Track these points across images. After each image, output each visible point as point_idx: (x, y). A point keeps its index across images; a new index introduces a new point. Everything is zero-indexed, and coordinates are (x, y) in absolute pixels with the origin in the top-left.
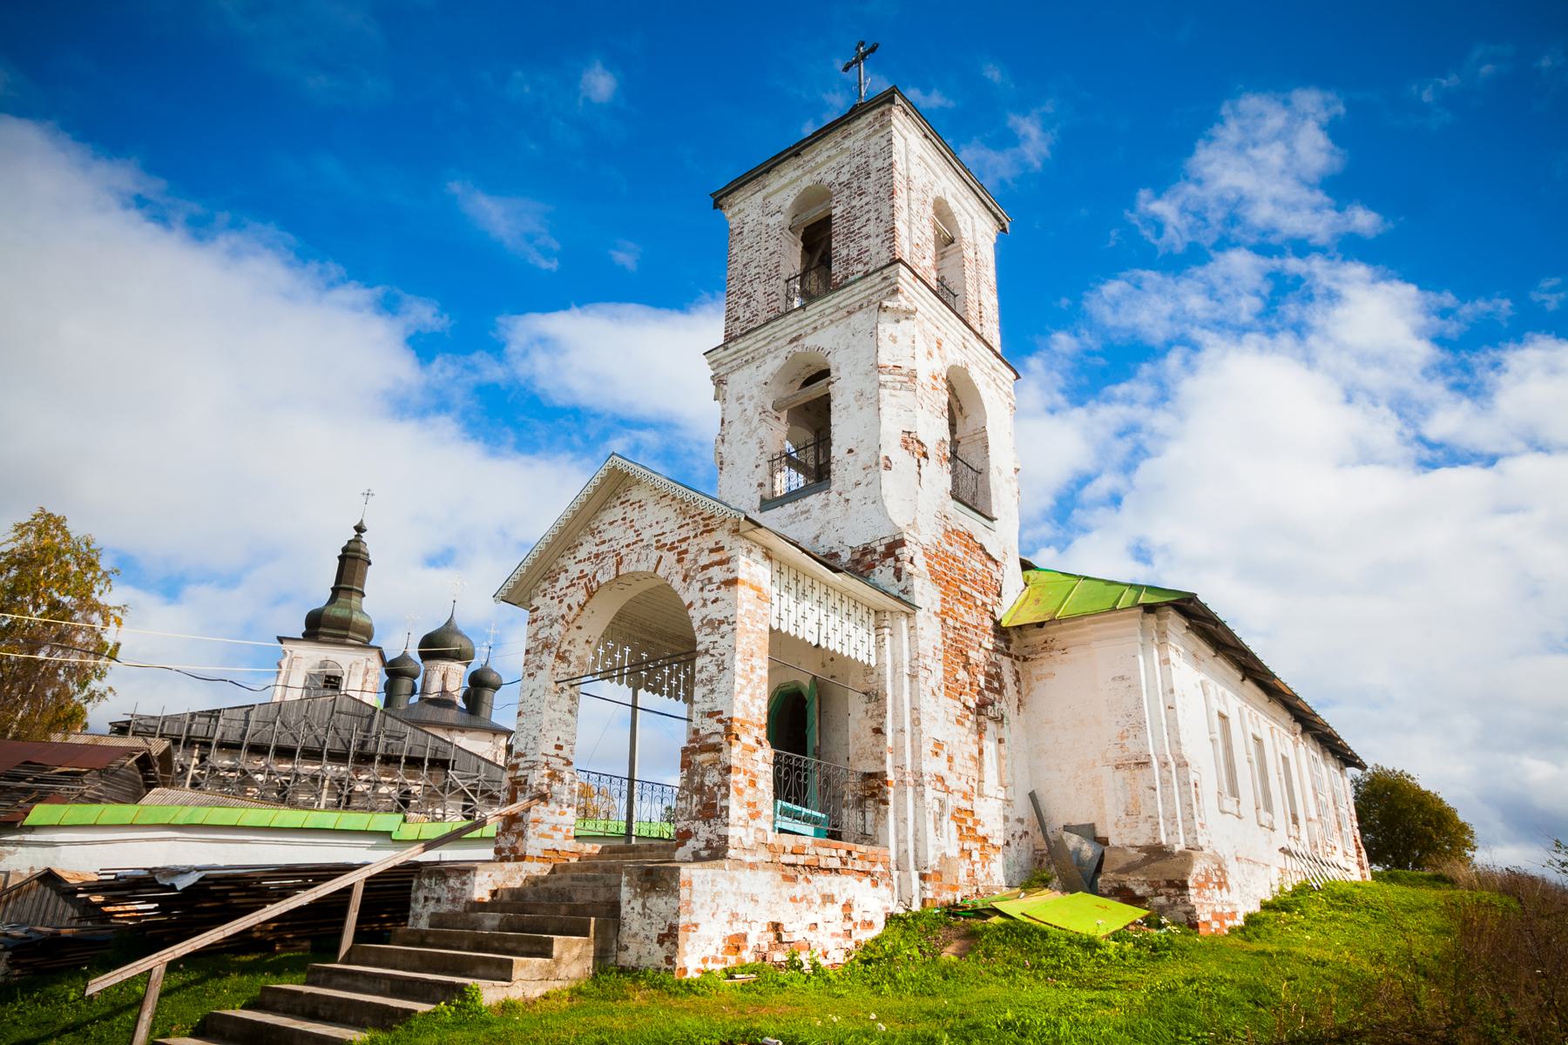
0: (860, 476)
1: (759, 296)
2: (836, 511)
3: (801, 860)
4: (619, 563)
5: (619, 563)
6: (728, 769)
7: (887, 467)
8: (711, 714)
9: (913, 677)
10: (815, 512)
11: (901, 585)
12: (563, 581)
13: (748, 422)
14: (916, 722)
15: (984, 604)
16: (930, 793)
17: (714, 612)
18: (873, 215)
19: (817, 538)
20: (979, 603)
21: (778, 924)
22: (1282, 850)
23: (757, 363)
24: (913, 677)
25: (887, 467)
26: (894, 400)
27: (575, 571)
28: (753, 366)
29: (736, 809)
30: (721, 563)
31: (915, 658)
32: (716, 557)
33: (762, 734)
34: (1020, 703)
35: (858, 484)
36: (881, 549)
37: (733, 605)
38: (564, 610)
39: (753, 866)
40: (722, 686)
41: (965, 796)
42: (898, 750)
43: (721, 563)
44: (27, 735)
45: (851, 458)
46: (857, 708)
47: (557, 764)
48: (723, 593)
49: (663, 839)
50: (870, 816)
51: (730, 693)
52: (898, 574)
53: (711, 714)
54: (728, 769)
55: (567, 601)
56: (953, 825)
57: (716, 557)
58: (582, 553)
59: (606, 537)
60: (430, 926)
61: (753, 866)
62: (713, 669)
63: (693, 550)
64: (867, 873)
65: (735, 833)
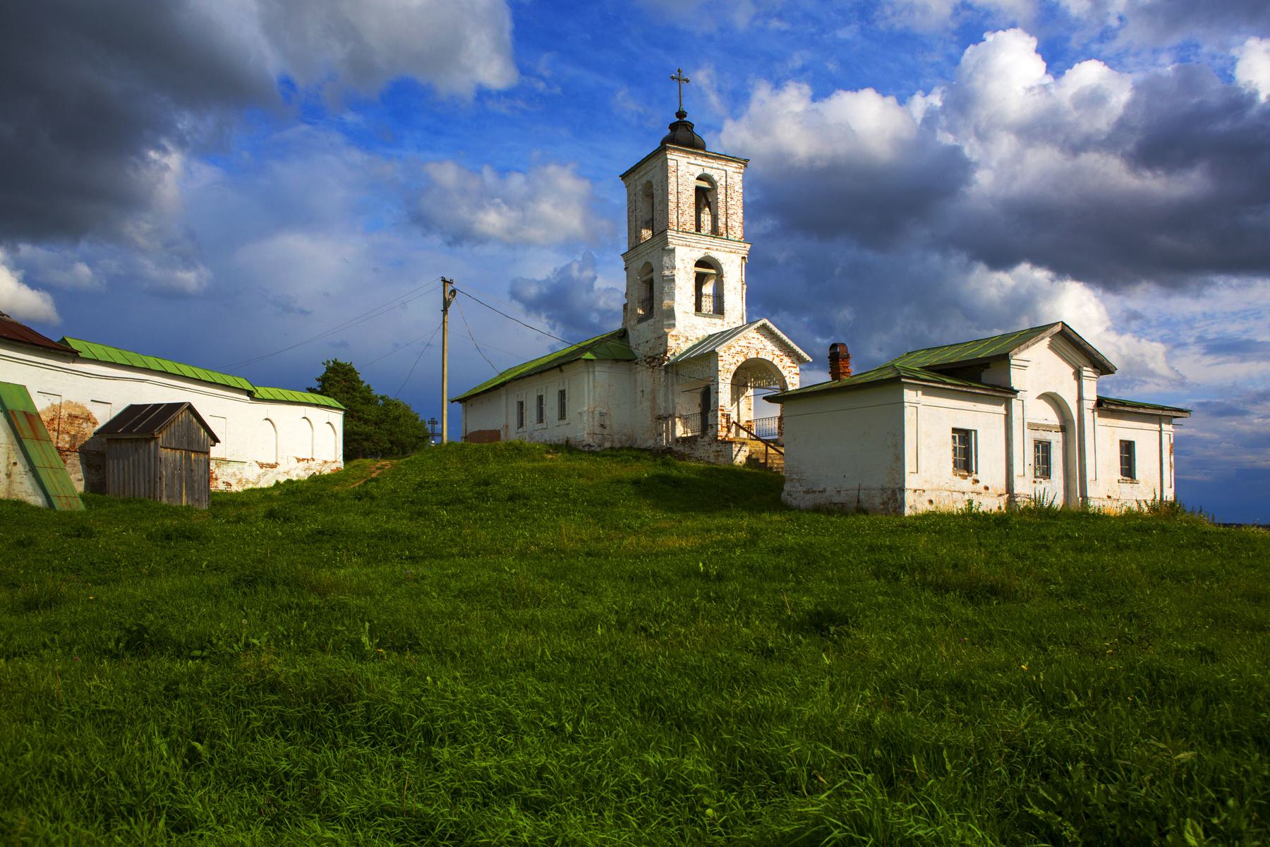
27: (739, 349)
28: (689, 249)
55: (736, 358)
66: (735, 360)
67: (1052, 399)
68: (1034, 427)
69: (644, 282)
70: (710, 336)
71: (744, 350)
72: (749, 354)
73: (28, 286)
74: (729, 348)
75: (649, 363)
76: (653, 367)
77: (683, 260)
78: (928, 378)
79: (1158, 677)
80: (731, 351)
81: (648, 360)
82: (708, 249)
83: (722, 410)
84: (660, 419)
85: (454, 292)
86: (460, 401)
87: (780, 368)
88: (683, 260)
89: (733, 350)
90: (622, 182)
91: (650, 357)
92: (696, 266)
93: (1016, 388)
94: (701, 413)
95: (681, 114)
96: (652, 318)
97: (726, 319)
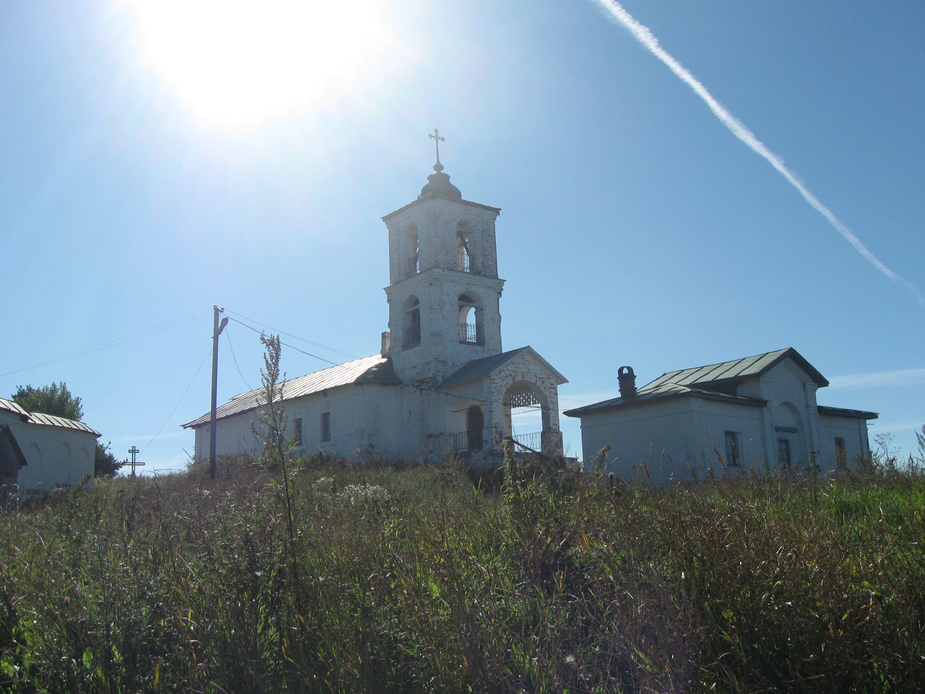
22: (374, 447)
27: (508, 373)
53: (555, 425)
55: (506, 381)
66: (505, 383)
67: (787, 404)
68: (778, 429)
69: (408, 313)
70: (473, 362)
71: (512, 374)
72: (516, 377)
73: (651, 31)
74: (500, 372)
75: (417, 387)
76: (422, 390)
77: (448, 294)
78: (655, 392)
79: (141, 522)
80: (502, 375)
81: (416, 384)
82: (469, 284)
83: (496, 427)
84: (431, 437)
85: (225, 321)
86: (193, 427)
87: (542, 389)
88: (448, 294)
89: (503, 374)
90: (384, 223)
91: (417, 381)
92: (459, 300)
93: (765, 399)
94: (467, 431)
95: (439, 167)
96: (419, 346)
97: (486, 347)
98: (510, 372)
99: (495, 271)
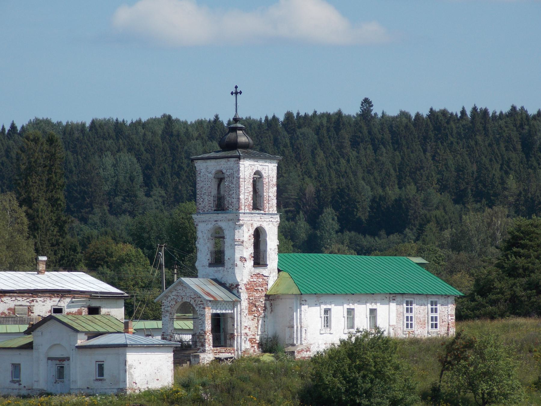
0: (231, 266)
1: (206, 200)
2: (226, 273)
3: (218, 351)
4: (182, 298)
5: (182, 298)
6: (205, 339)
7: (236, 266)
8: (202, 330)
9: (240, 314)
10: (221, 272)
11: (239, 294)
12: (169, 299)
13: (204, 240)
14: (241, 323)
15: (262, 290)
16: (243, 337)
17: (202, 313)
18: (235, 191)
19: (222, 278)
20: (260, 290)
21: (32, 348)
23: (206, 223)
24: (240, 314)
25: (236, 266)
26: (238, 248)
27: (172, 297)
29: (207, 345)
30: (202, 304)
31: (241, 310)
32: (201, 303)
33: (210, 332)
34: (272, 311)
35: (230, 268)
36: (235, 285)
37: (205, 312)
38: (171, 305)
39: (210, 353)
40: (204, 326)
41: (253, 335)
42: (237, 329)
43: (202, 304)
44: (274, 372)
45: (228, 260)
46: (229, 320)
47: (171, 334)
48: (203, 310)
49: (178, 334)
50: (232, 341)
51: (205, 327)
52: (238, 291)
53: (202, 330)
54: (205, 339)
55: (171, 303)
56: (249, 342)
57: (201, 303)
58: (174, 294)
59: (179, 292)
60: (199, 355)
61: (210, 353)
62: (202, 322)
63: (197, 300)
64: (230, 352)
65: (207, 349)
77: (202, 232)
87: (194, 306)
98: (174, 296)
99: (237, 205)
